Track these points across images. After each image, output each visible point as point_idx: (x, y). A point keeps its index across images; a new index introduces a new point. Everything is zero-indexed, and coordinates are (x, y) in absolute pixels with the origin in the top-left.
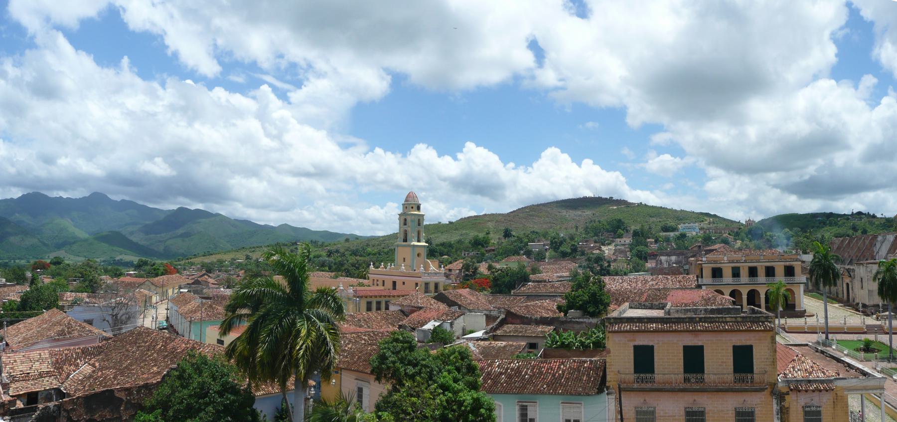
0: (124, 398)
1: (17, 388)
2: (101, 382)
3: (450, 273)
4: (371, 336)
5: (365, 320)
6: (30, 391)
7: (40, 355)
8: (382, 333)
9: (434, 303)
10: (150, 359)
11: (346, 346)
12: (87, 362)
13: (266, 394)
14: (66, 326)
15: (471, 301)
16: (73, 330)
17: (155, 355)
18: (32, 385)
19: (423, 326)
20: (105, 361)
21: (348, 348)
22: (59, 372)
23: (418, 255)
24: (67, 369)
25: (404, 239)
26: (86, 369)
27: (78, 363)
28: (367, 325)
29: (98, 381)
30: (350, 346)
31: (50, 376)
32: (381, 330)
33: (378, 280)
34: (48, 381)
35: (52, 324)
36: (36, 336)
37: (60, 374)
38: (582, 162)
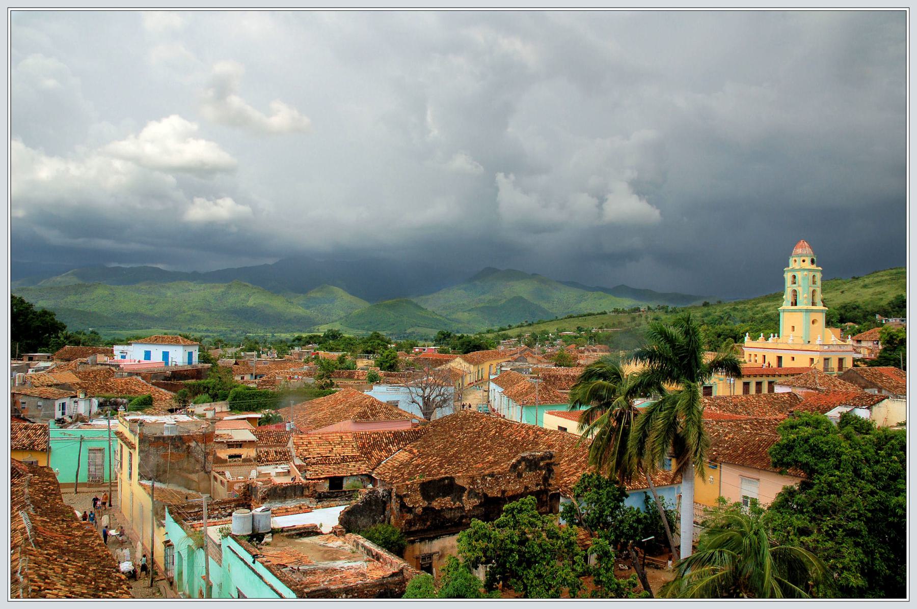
0: (467, 487)
1: (315, 471)
2: (423, 471)
3: (859, 345)
4: (754, 425)
5: (742, 405)
6: (333, 475)
7: (342, 438)
8: (769, 421)
10: (482, 447)
11: (726, 436)
12: (401, 448)
13: (633, 489)
14: (368, 407)
15: (898, 383)
16: (378, 413)
17: (489, 442)
18: (334, 469)
19: (826, 411)
20: (424, 448)
21: (729, 438)
22: (367, 458)
23: (813, 322)
24: (377, 454)
25: (792, 303)
26: (402, 456)
27: (390, 449)
28: (746, 411)
29: (420, 469)
30: (731, 436)
31: (357, 461)
32: (767, 417)
33: (756, 355)
34: (354, 466)
35: (350, 405)
36: (329, 417)
37: (369, 459)
38: (222, 270)
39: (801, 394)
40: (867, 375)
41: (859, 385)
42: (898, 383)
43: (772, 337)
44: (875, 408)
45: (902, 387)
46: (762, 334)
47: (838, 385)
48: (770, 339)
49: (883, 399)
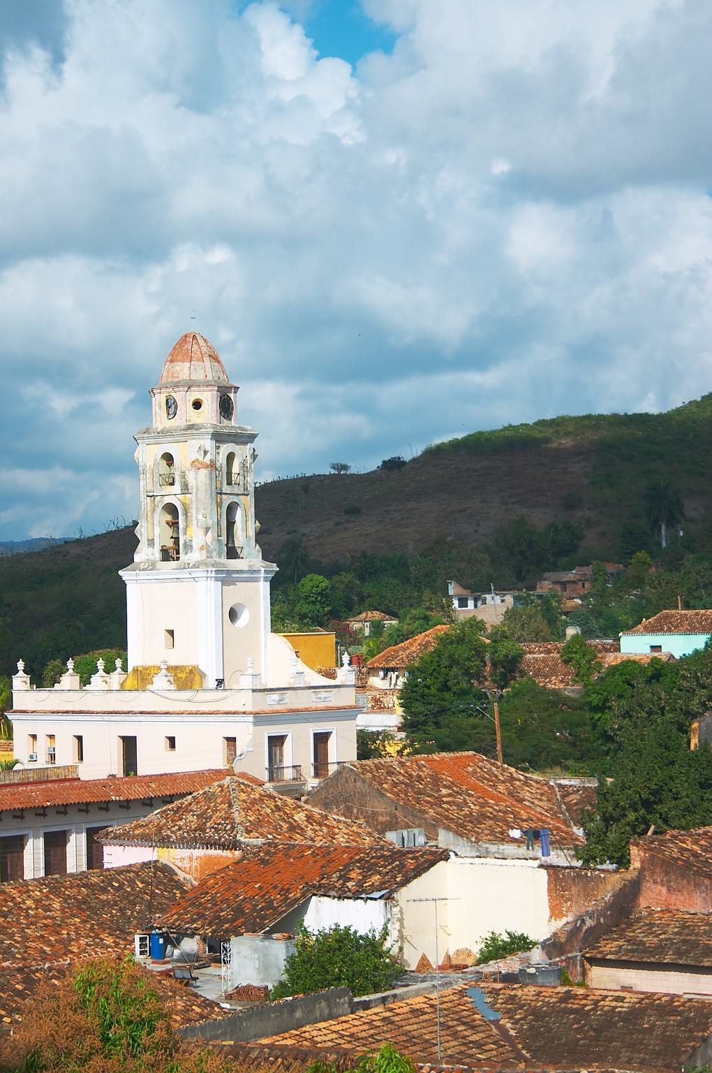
9: (309, 818)
39: (186, 864)
40: (395, 785)
41: (371, 819)
42: (482, 806)
43: (101, 672)
44: (403, 894)
45: (494, 818)
46: (21, 665)
47: (303, 824)
48: (94, 679)
49: (433, 864)
